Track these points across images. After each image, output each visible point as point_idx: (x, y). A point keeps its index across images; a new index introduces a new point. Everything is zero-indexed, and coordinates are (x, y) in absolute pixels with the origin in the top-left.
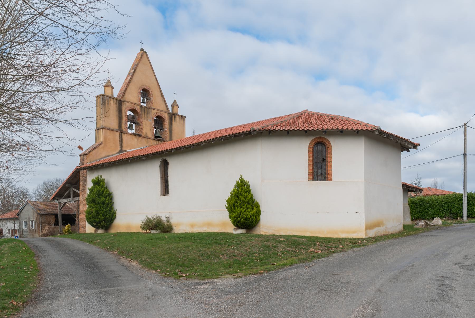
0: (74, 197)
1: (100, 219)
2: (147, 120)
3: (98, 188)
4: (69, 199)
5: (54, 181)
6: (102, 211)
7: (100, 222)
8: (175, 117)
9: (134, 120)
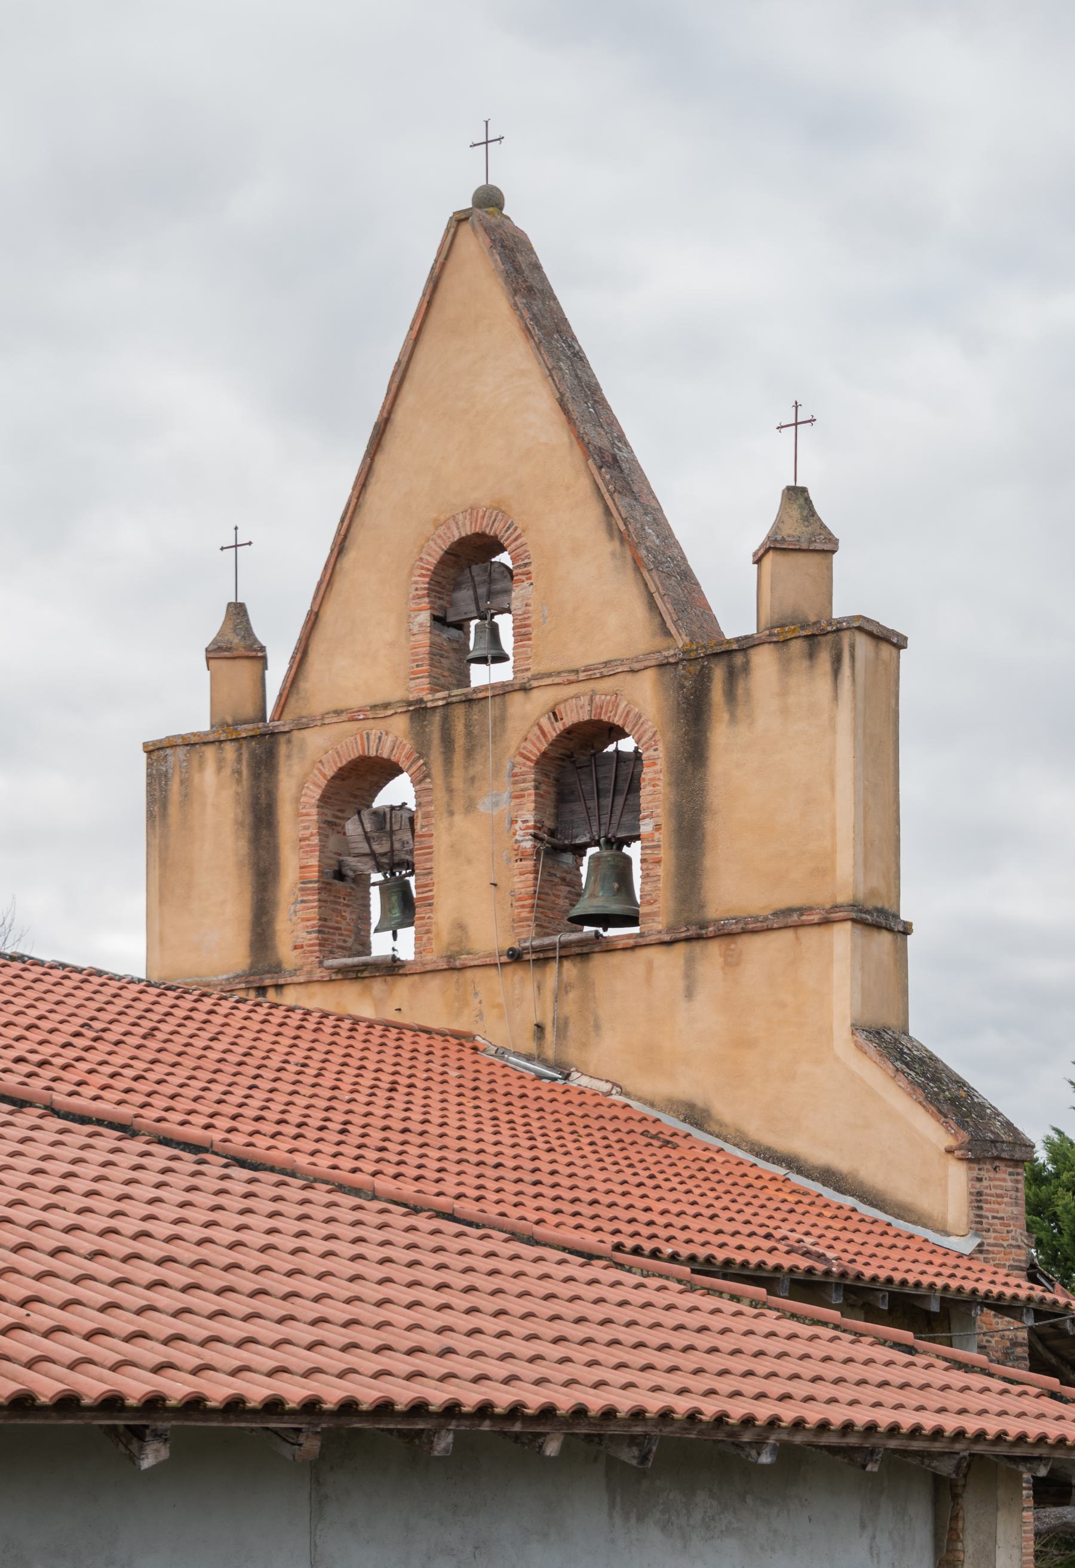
9: (397, 846)
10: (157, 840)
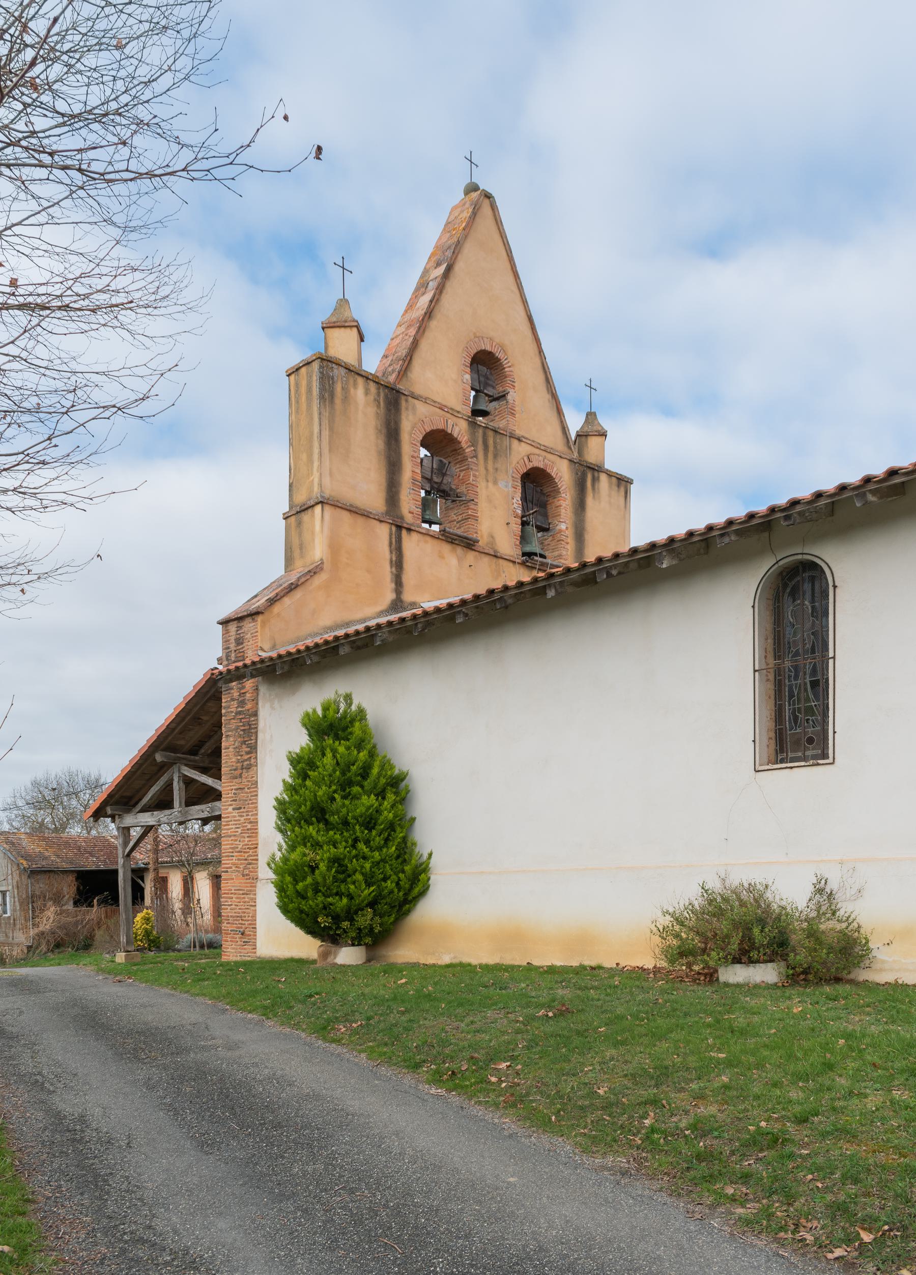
0: (190, 802)
1: (351, 897)
2: (495, 482)
3: (341, 749)
4: (167, 812)
5: (63, 776)
6: (365, 858)
7: (350, 915)
8: (595, 480)
9: (445, 481)
10: (327, 414)
